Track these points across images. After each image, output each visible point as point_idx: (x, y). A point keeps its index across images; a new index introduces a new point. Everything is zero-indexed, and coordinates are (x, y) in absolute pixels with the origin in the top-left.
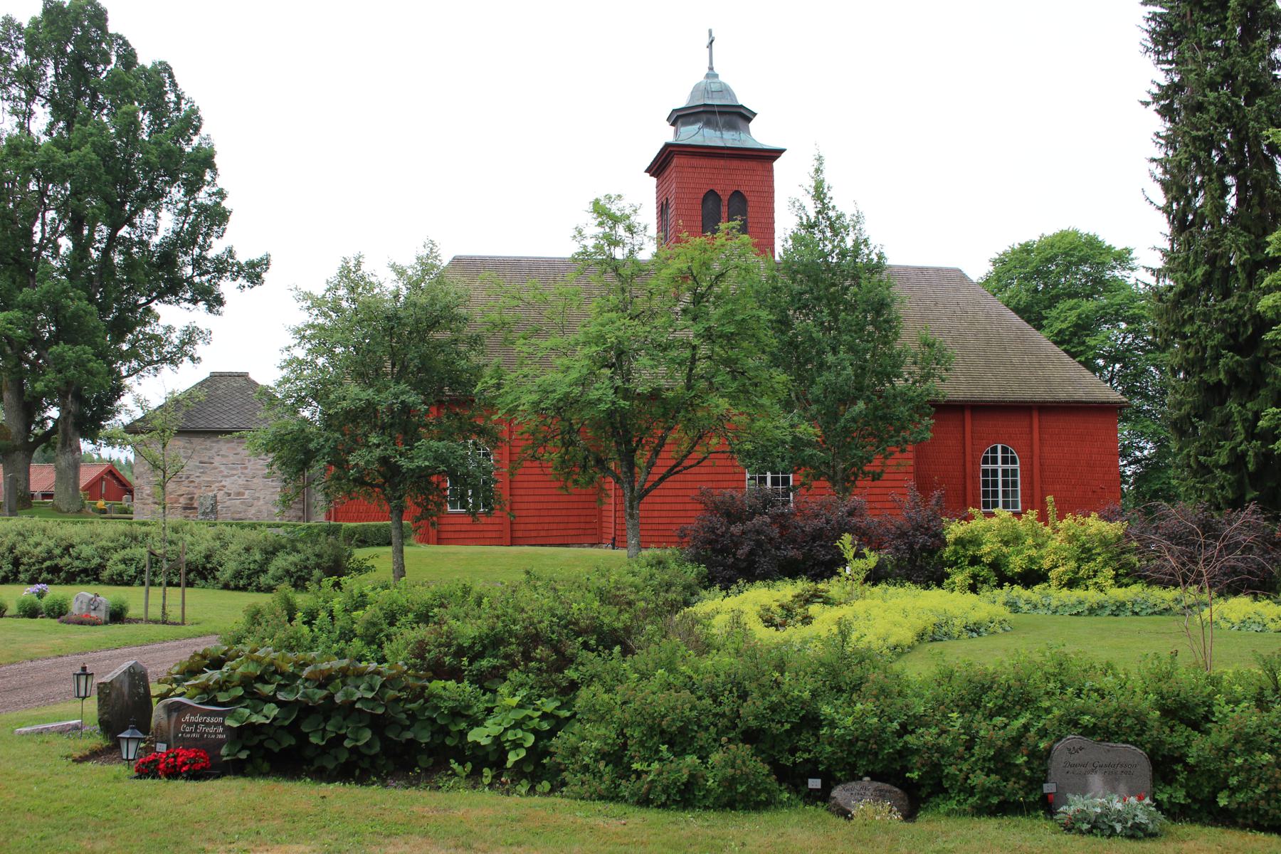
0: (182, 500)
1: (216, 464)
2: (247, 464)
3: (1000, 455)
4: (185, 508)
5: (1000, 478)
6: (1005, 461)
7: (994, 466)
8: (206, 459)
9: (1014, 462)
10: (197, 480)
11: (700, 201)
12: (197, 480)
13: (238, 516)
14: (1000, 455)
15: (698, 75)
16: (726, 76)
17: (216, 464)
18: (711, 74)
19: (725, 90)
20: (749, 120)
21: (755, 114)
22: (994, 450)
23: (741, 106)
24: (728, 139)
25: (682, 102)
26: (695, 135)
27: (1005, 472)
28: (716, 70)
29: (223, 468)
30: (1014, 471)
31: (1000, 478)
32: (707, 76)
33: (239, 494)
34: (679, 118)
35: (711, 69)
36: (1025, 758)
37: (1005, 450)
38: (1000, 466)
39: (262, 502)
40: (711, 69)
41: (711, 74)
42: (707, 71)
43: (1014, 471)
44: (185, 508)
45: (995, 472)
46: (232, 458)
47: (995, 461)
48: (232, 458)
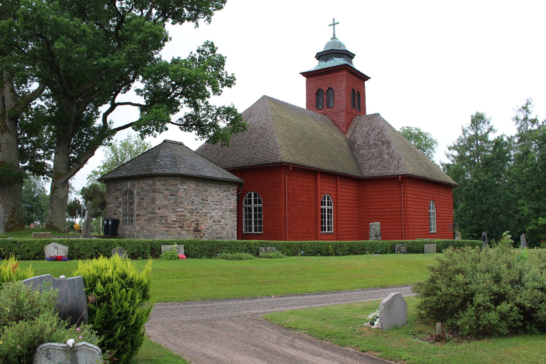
1: (209, 201)
2: (223, 202)
4: (195, 231)
8: (204, 198)
9: (260, 203)
10: (201, 211)
11: (315, 96)
12: (201, 211)
13: (219, 236)
15: (328, 39)
18: (334, 38)
19: (340, 44)
20: (352, 58)
21: (355, 55)
22: (250, 196)
23: (347, 51)
25: (321, 50)
27: (255, 209)
28: (336, 36)
30: (331, 209)
32: (332, 39)
33: (219, 221)
34: (320, 56)
35: (334, 35)
36: (35, 222)
39: (229, 227)
40: (334, 35)
41: (334, 38)
42: (332, 36)
44: (195, 231)
45: (255, 203)
46: (216, 198)
47: (250, 203)
48: (216, 198)
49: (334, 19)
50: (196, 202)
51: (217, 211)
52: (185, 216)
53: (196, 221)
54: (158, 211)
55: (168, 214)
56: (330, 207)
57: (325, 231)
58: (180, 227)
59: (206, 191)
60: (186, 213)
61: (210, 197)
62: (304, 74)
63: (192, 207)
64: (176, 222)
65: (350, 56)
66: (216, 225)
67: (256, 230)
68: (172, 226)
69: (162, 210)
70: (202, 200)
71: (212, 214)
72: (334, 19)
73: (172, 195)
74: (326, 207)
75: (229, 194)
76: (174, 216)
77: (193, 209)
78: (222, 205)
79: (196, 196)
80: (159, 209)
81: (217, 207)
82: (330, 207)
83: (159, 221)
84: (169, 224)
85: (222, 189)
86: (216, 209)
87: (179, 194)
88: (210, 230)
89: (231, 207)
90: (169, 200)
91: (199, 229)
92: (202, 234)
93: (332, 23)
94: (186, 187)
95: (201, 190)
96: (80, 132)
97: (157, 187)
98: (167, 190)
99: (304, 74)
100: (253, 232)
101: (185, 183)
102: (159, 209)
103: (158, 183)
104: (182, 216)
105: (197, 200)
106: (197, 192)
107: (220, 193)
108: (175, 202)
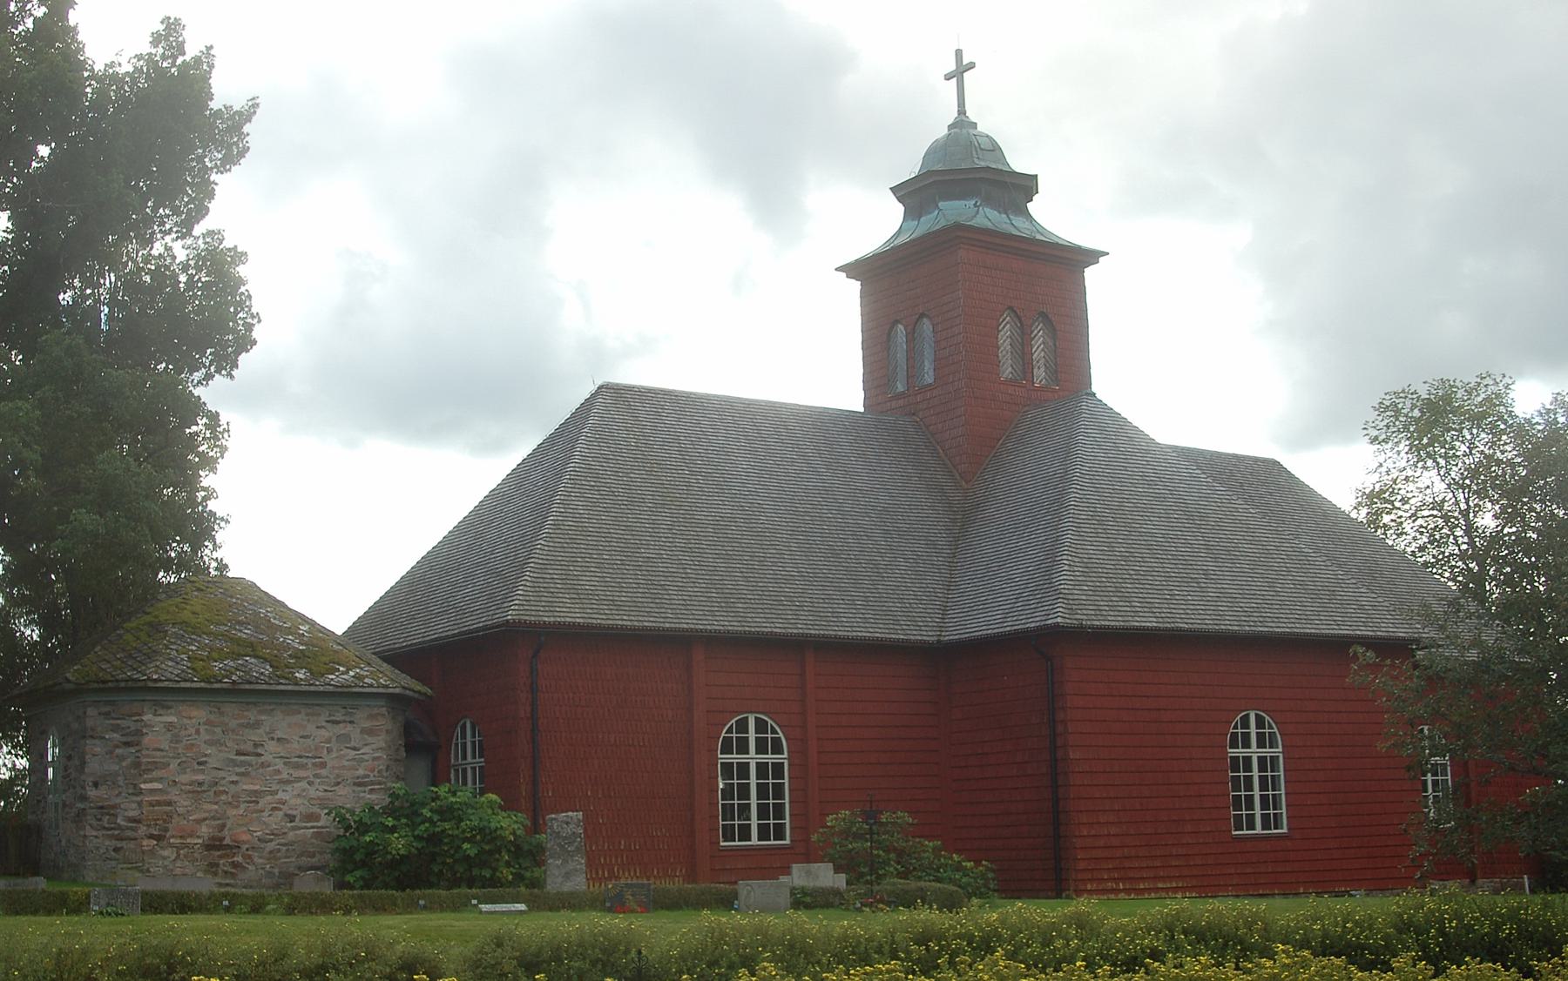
0: (204, 830)
1: (267, 758)
3: (752, 735)
5: (753, 781)
6: (761, 748)
7: (763, 758)
8: (249, 747)
9: (777, 749)
14: (752, 735)
16: (988, 121)
17: (267, 758)
18: (962, 123)
22: (742, 726)
24: (990, 218)
26: (956, 210)
27: (762, 769)
28: (972, 115)
29: (279, 764)
30: (1274, 759)
31: (753, 781)
35: (962, 111)
37: (761, 726)
38: (753, 758)
40: (962, 111)
41: (962, 123)
42: (952, 115)
43: (778, 768)
47: (743, 747)
49: (959, 53)
50: (212, 762)
51: (304, 784)
52: (169, 803)
53: (213, 818)
54: (92, 793)
55: (118, 801)
56: (1267, 752)
57: (1251, 826)
58: (151, 837)
59: (257, 725)
60: (173, 795)
61: (271, 746)
62: (851, 270)
63: (200, 777)
64: (138, 821)
65: (1026, 186)
66: (294, 829)
67: (1265, 826)
68: (129, 833)
69: (102, 792)
70: (239, 753)
71: (280, 795)
72: (959, 53)
73: (127, 744)
74: (1254, 752)
75: (354, 732)
76: (134, 806)
77: (200, 784)
78: (323, 765)
79: (210, 743)
80: (96, 785)
81: (302, 773)
82: (1267, 752)
83: (94, 822)
84: (119, 827)
85: (323, 718)
86: (299, 779)
87: (146, 740)
88: (271, 846)
89: (361, 772)
90: (122, 758)
91: (227, 841)
92: (239, 859)
93: (953, 67)
94: (173, 719)
95: (233, 723)
96: (1544, 604)
97: (89, 723)
98: (116, 728)
99: (851, 270)
100: (754, 841)
101: (169, 708)
102: (96, 785)
103: (91, 711)
104: (159, 803)
105: (215, 756)
106: (218, 730)
107: (311, 728)
108: (137, 765)
